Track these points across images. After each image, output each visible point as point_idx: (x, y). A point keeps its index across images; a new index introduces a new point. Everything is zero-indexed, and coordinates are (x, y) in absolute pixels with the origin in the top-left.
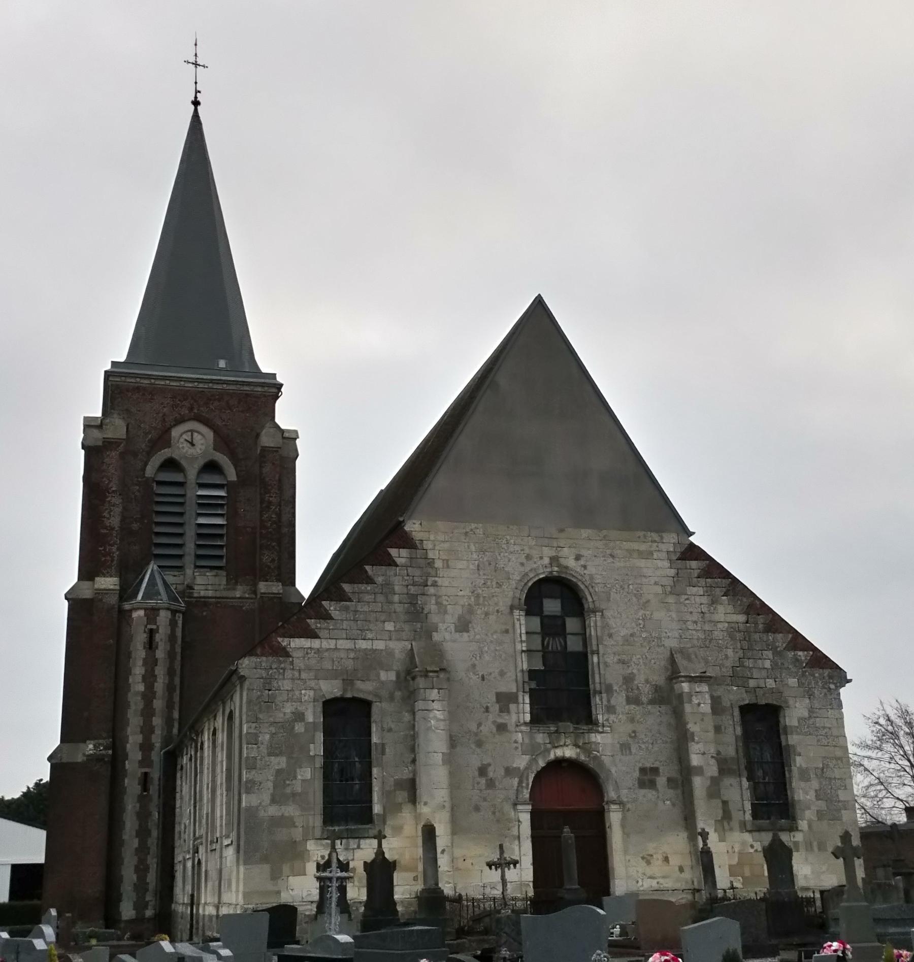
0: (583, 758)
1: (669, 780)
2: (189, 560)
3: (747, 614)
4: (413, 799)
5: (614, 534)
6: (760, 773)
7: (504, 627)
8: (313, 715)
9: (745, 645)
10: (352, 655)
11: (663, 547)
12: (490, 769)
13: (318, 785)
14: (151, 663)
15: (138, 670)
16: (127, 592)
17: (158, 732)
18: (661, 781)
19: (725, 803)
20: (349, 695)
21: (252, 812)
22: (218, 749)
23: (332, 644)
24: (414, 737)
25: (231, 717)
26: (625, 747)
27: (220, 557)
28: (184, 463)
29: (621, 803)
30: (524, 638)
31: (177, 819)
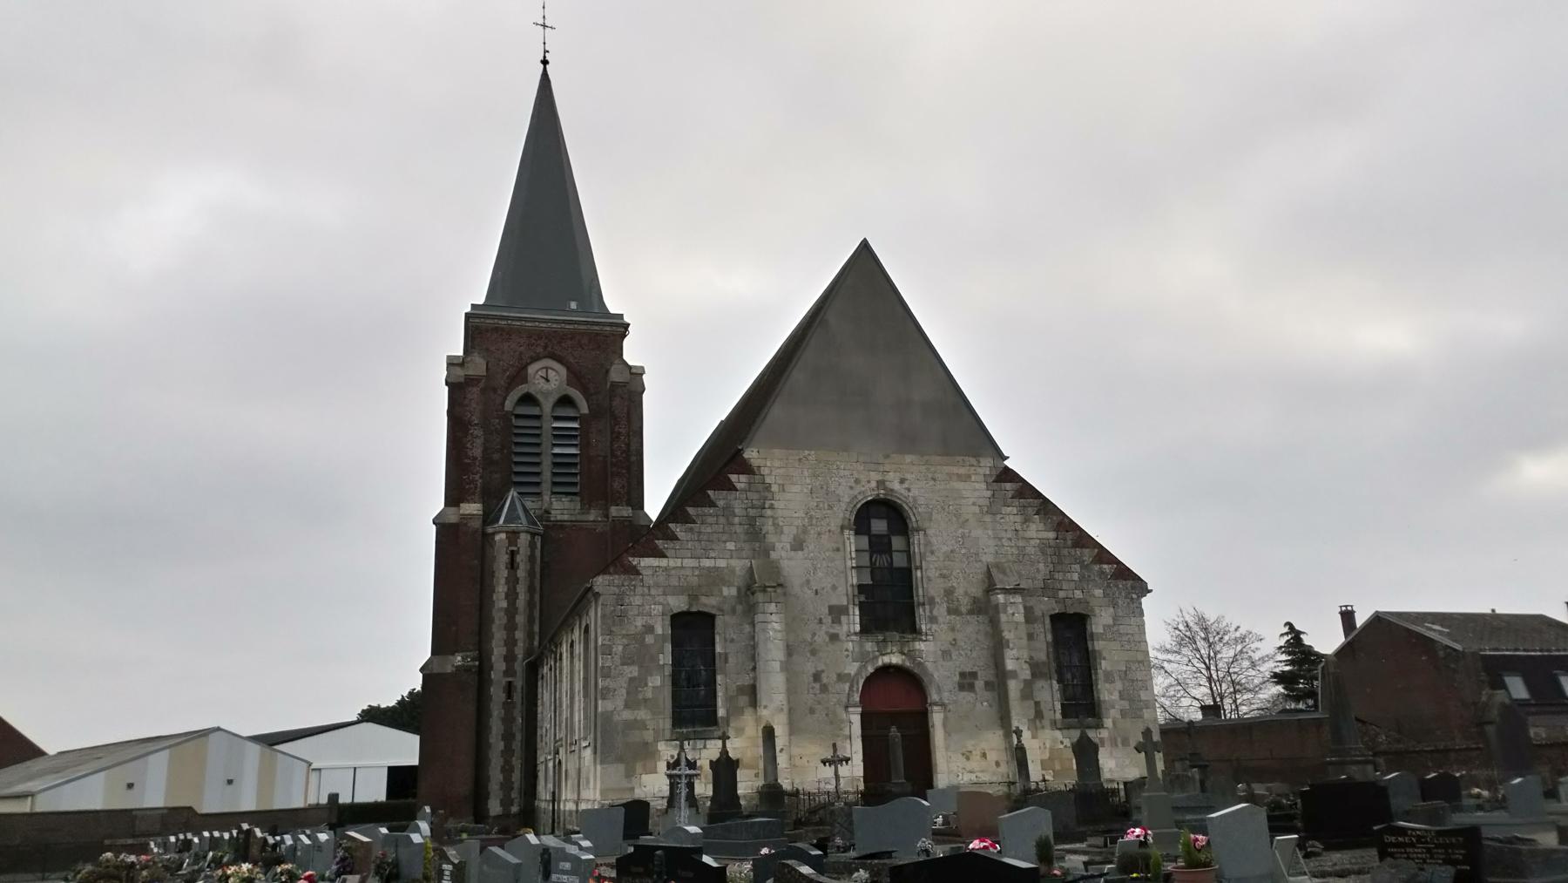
1: (987, 684)
2: (546, 488)
4: (754, 703)
6: (1069, 676)
8: (662, 628)
9: (1055, 559)
14: (512, 581)
15: (501, 588)
16: (489, 517)
17: (520, 644)
18: (979, 684)
19: (1037, 704)
21: (607, 716)
23: (678, 562)
24: (754, 647)
26: (946, 654)
27: (574, 484)
28: (539, 397)
29: (943, 705)
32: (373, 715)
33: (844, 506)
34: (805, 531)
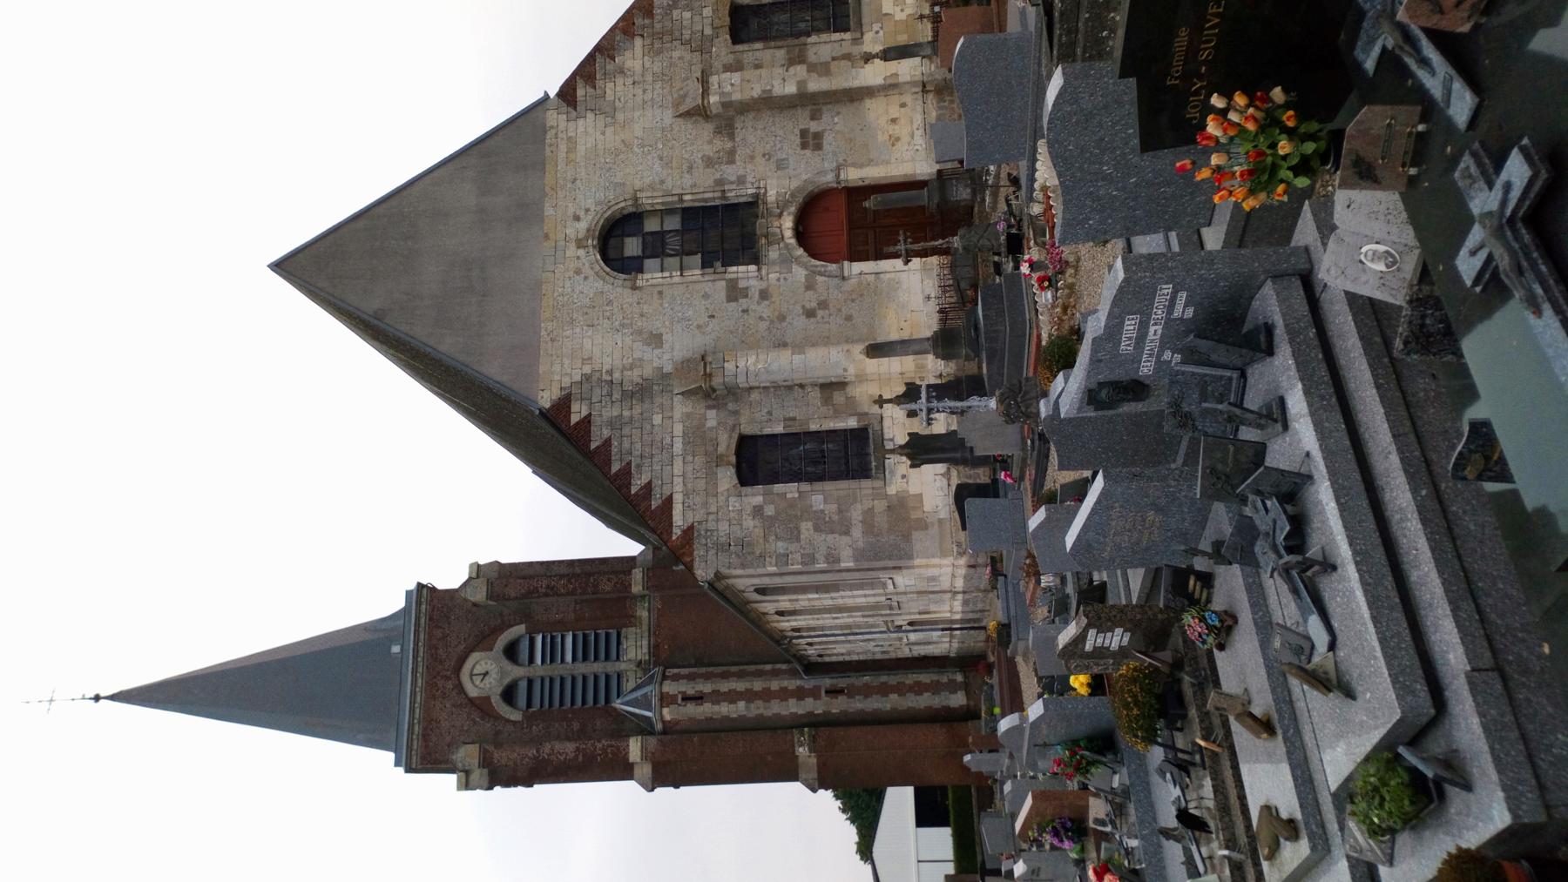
0: (793, 209)
1: (812, 119)
2: (611, 667)
3: (633, 36)
4: (841, 385)
5: (549, 179)
6: (802, 25)
7: (656, 296)
8: (755, 496)
9: (667, 38)
10: (690, 458)
11: (562, 125)
12: (808, 306)
13: (829, 486)
14: (717, 697)
15: (725, 709)
16: (644, 728)
17: (785, 683)
18: (814, 127)
19: (834, 59)
20: (733, 459)
21: (859, 555)
22: (798, 606)
23: (678, 480)
24: (777, 387)
25: (762, 591)
26: (781, 165)
27: (608, 635)
28: (507, 681)
29: (838, 168)
30: (666, 274)
31: (870, 657)
32: (865, 850)
33: (608, 287)
34: (640, 332)
